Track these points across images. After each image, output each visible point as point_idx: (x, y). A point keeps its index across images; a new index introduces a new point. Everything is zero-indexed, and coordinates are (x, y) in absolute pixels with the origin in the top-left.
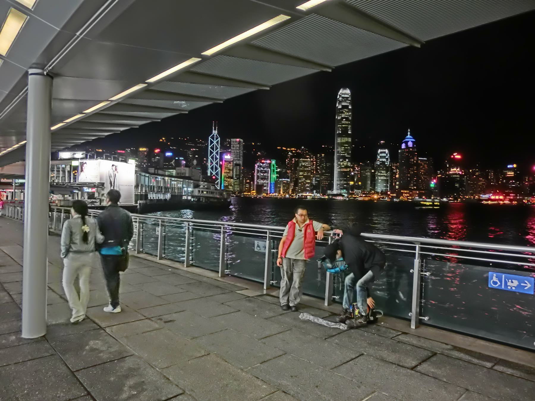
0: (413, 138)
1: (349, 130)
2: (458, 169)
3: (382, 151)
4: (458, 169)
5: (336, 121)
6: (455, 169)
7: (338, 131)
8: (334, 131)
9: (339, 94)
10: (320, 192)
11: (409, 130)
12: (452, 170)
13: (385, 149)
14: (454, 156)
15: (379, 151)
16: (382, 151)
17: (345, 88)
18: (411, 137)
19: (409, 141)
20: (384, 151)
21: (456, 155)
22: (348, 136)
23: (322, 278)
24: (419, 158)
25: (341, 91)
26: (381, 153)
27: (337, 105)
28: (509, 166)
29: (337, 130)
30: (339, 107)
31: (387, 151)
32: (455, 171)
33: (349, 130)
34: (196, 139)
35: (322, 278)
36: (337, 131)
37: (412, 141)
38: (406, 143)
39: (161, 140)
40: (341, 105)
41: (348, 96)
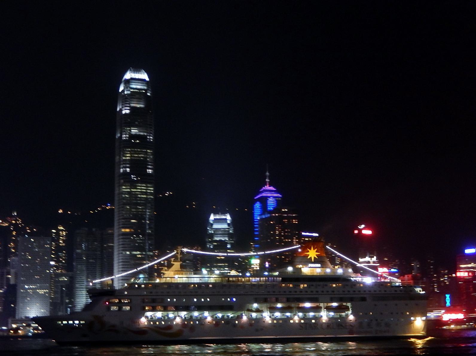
1: (150, 167)
2: (374, 259)
3: (218, 217)
4: (374, 259)
5: (117, 144)
6: (367, 259)
7: (124, 167)
8: (112, 166)
10: (132, 158)
11: (268, 174)
13: (224, 213)
14: (360, 230)
15: (212, 217)
16: (218, 217)
17: (137, 69)
18: (272, 188)
19: (269, 197)
20: (223, 217)
21: (364, 229)
22: (145, 179)
23: (110, 250)
24: (303, 234)
25: (128, 75)
26: (216, 220)
28: (468, 251)
29: (120, 165)
30: (124, 112)
31: (228, 217)
33: (150, 167)
34: (271, 231)
35: (110, 250)
36: (120, 168)
38: (264, 201)
39: (356, 232)
40: (128, 108)
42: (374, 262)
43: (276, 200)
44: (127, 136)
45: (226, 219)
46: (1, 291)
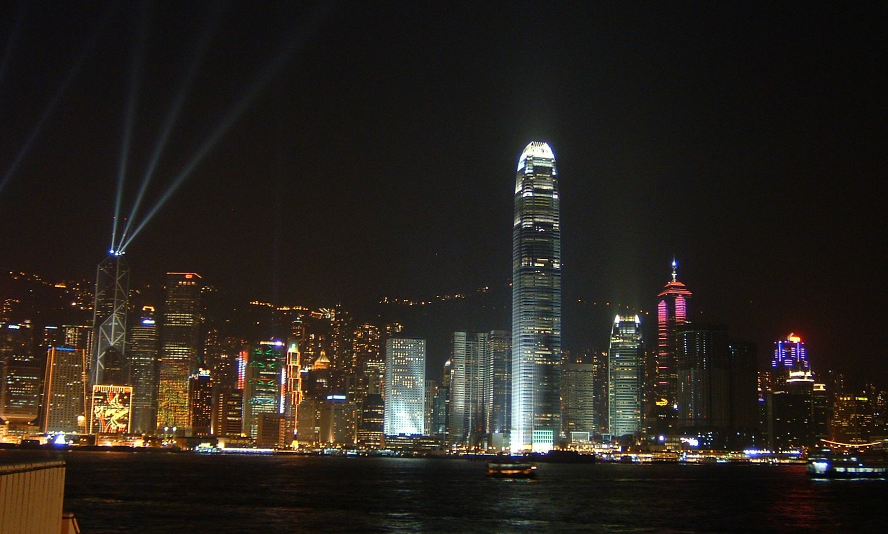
0: (687, 288)
2: (809, 374)
9: (523, 157)
12: (792, 374)
27: (518, 188)
32: (803, 377)
37: (683, 295)
41: (550, 165)
42: (809, 378)
43: (685, 298)
44: (531, 223)
45: (634, 323)
46: (887, 424)
